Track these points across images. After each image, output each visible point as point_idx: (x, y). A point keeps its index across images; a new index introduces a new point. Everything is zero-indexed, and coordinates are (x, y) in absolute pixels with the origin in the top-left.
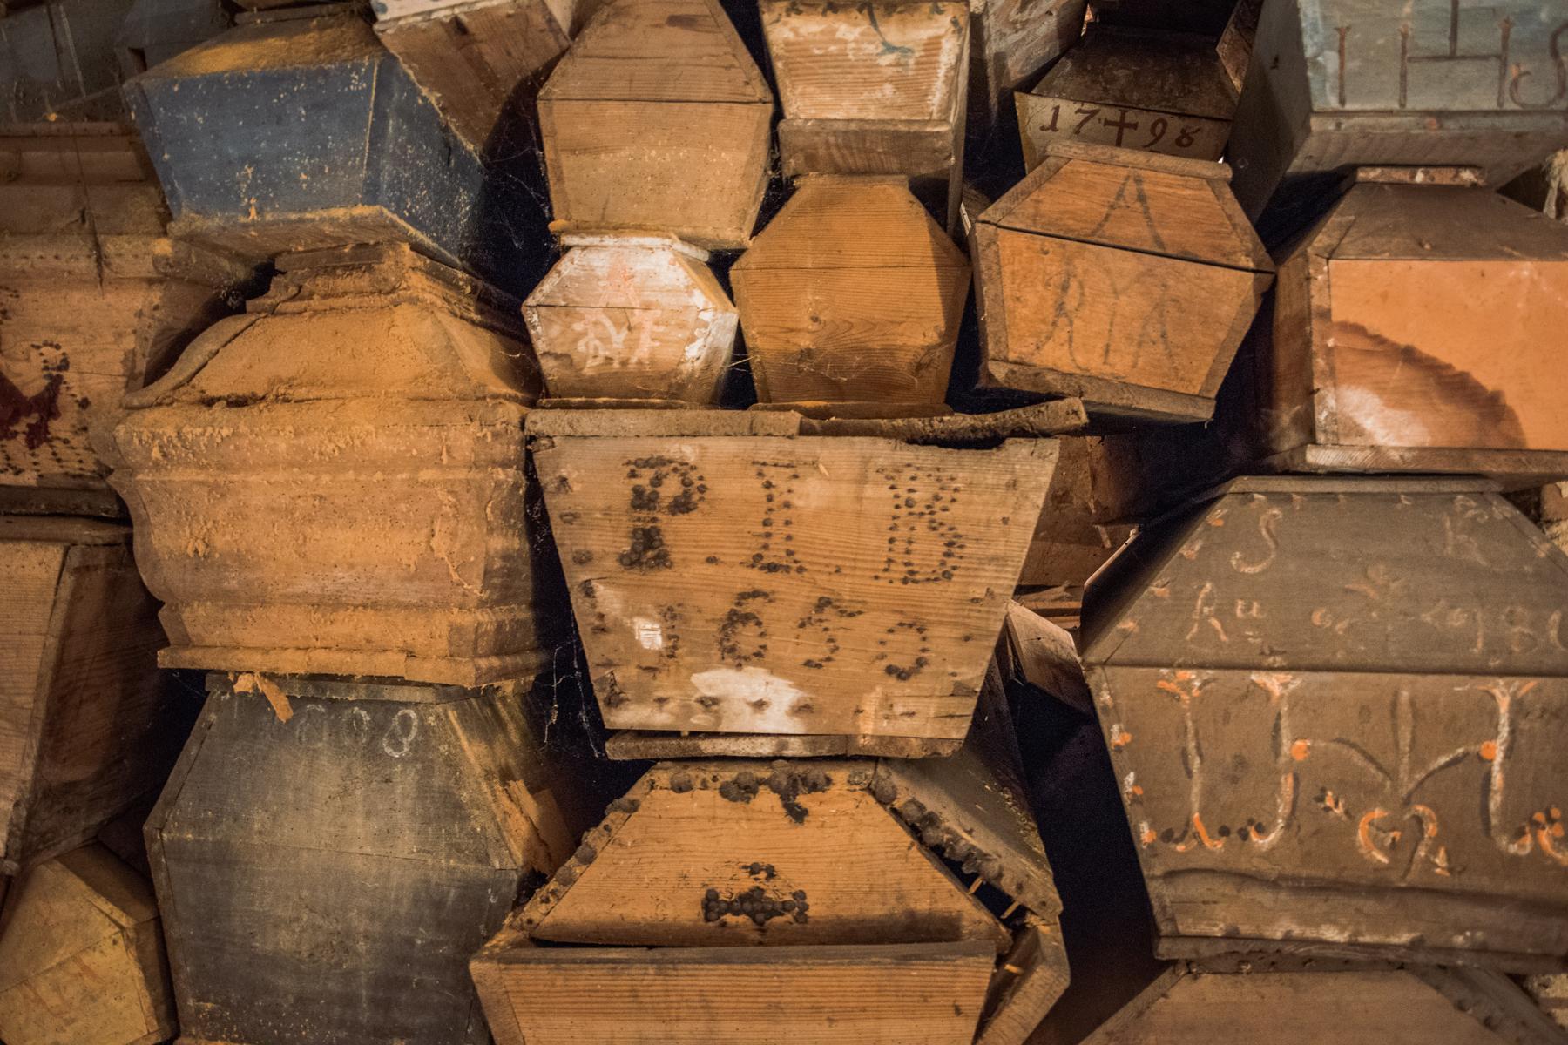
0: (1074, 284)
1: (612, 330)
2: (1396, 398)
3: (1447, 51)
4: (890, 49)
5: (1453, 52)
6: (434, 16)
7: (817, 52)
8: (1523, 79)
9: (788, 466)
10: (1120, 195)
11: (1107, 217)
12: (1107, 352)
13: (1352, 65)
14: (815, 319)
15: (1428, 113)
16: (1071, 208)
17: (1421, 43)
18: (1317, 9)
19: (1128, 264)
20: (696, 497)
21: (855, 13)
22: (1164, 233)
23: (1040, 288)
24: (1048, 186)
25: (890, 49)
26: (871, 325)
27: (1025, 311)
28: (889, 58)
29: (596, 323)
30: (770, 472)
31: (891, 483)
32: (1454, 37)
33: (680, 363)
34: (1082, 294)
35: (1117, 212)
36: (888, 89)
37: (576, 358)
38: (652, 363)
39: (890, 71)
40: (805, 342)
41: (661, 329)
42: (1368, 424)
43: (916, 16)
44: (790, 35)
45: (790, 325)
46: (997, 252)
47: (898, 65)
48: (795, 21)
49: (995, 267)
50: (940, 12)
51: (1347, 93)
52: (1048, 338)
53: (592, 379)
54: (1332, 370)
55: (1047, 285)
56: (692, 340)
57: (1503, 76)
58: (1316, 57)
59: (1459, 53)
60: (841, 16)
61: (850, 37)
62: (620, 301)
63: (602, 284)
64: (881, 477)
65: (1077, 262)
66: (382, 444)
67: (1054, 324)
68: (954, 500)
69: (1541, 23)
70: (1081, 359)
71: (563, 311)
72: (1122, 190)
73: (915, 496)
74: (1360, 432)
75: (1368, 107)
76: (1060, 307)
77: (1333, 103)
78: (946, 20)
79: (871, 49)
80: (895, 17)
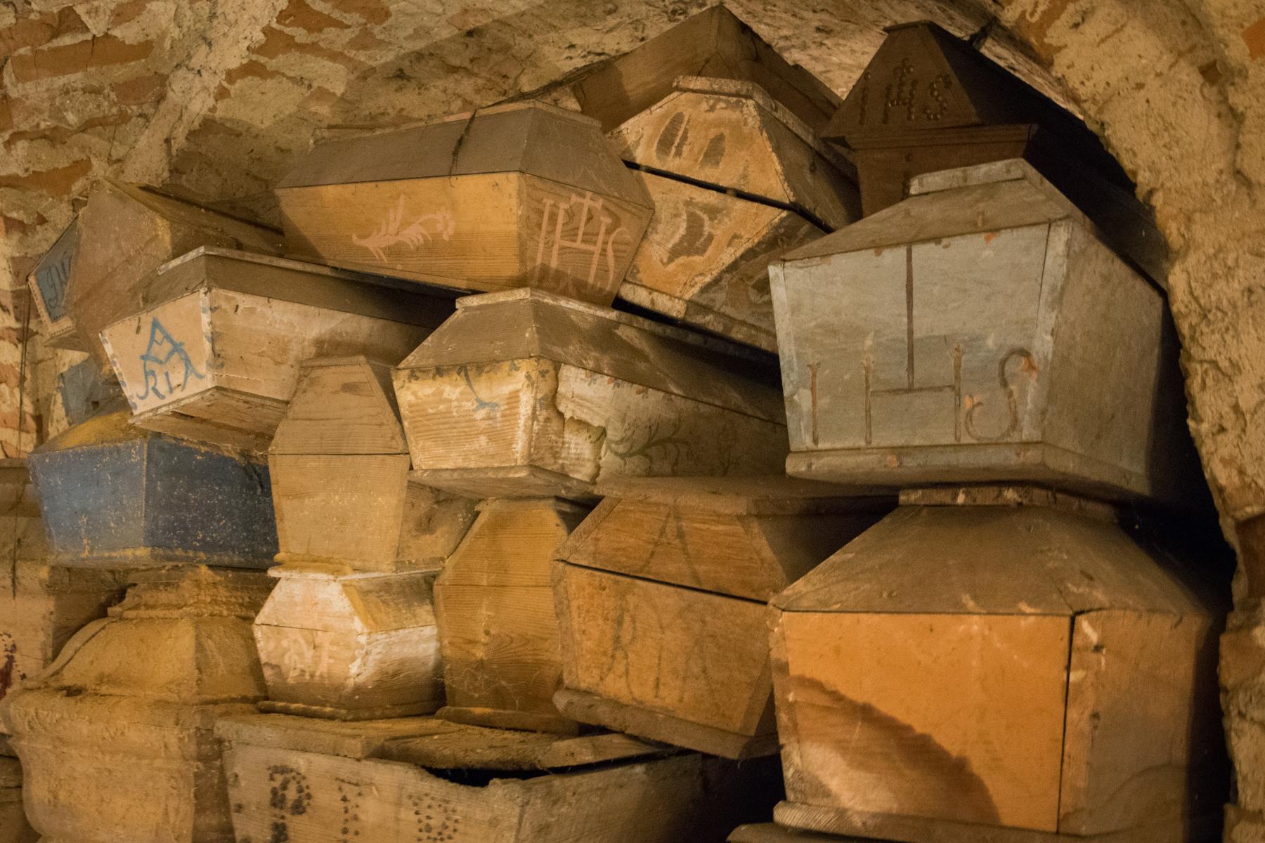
0: (627, 619)
1: (305, 647)
2: (859, 758)
3: (906, 386)
4: (482, 404)
5: (911, 385)
6: (160, 411)
7: (431, 411)
8: (977, 410)
9: (357, 785)
10: (662, 532)
11: (653, 553)
12: (657, 686)
13: (824, 402)
14: (487, 633)
15: (893, 449)
16: (622, 545)
17: (882, 376)
18: (793, 347)
19: (669, 599)
20: (305, 802)
21: (455, 376)
22: (701, 569)
23: (600, 622)
24: (605, 524)
25: (482, 404)
26: (527, 641)
27: (589, 643)
28: (481, 414)
29: (295, 641)
30: (346, 787)
31: (416, 808)
32: (911, 368)
33: (346, 678)
34: (635, 628)
35: (659, 549)
36: (483, 440)
37: (284, 669)
38: (330, 677)
39: (483, 425)
40: (480, 653)
41: (335, 648)
42: (834, 784)
43: (499, 375)
44: (411, 398)
45: (471, 637)
46: (565, 588)
47: (489, 418)
48: (415, 385)
49: (565, 602)
50: (517, 369)
51: (820, 433)
52: (609, 670)
53: (293, 688)
54: (795, 725)
55: (606, 619)
56: (353, 659)
57: (958, 407)
58: (792, 395)
59: (916, 386)
60: (446, 378)
61: (454, 397)
62: (308, 624)
63: (298, 609)
64: (410, 802)
65: (629, 597)
66: (135, 736)
67: (613, 657)
68: (455, 830)
69: (989, 351)
70: (637, 692)
71: (275, 629)
72: (664, 528)
73: (432, 822)
74: (827, 794)
75: (838, 446)
76: (617, 639)
77: (808, 442)
78: (521, 375)
79: (468, 405)
80: (484, 376)
